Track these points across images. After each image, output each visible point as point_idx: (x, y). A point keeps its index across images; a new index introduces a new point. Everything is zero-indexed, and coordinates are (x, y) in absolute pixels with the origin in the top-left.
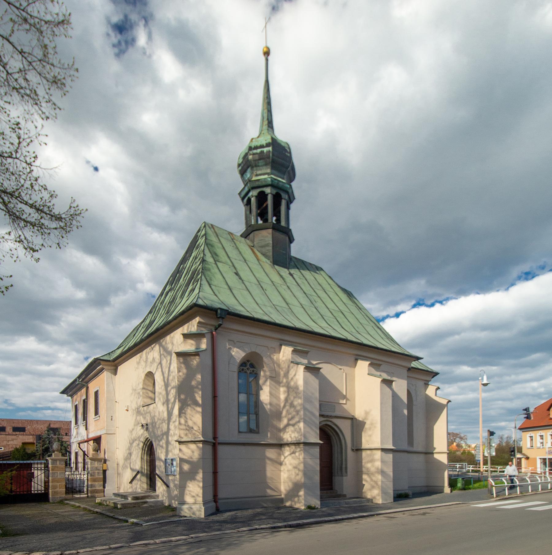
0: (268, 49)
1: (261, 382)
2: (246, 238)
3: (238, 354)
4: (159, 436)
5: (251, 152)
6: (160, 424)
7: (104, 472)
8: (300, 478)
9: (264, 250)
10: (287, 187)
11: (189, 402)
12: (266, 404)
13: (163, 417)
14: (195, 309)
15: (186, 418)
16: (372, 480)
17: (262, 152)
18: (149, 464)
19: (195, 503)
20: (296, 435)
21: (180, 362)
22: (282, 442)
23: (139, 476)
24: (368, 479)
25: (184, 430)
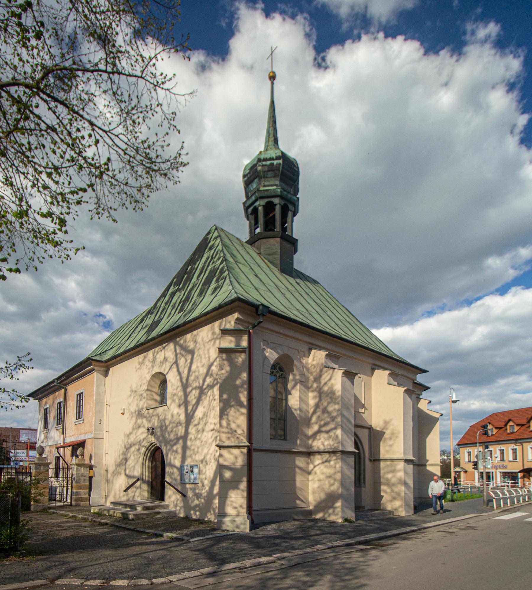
0: (274, 73)
1: (289, 386)
2: (251, 245)
3: (271, 355)
4: (171, 440)
5: (260, 164)
6: (173, 428)
7: (91, 478)
8: (336, 487)
9: (271, 258)
10: (294, 200)
11: (233, 403)
12: (296, 410)
13: (178, 420)
14: (237, 303)
15: (229, 421)
16: (392, 491)
17: (272, 164)
18: (150, 470)
19: (238, 515)
20: (331, 442)
21: (222, 358)
22: (311, 450)
23: (138, 484)
24: (389, 490)
25: (226, 433)
